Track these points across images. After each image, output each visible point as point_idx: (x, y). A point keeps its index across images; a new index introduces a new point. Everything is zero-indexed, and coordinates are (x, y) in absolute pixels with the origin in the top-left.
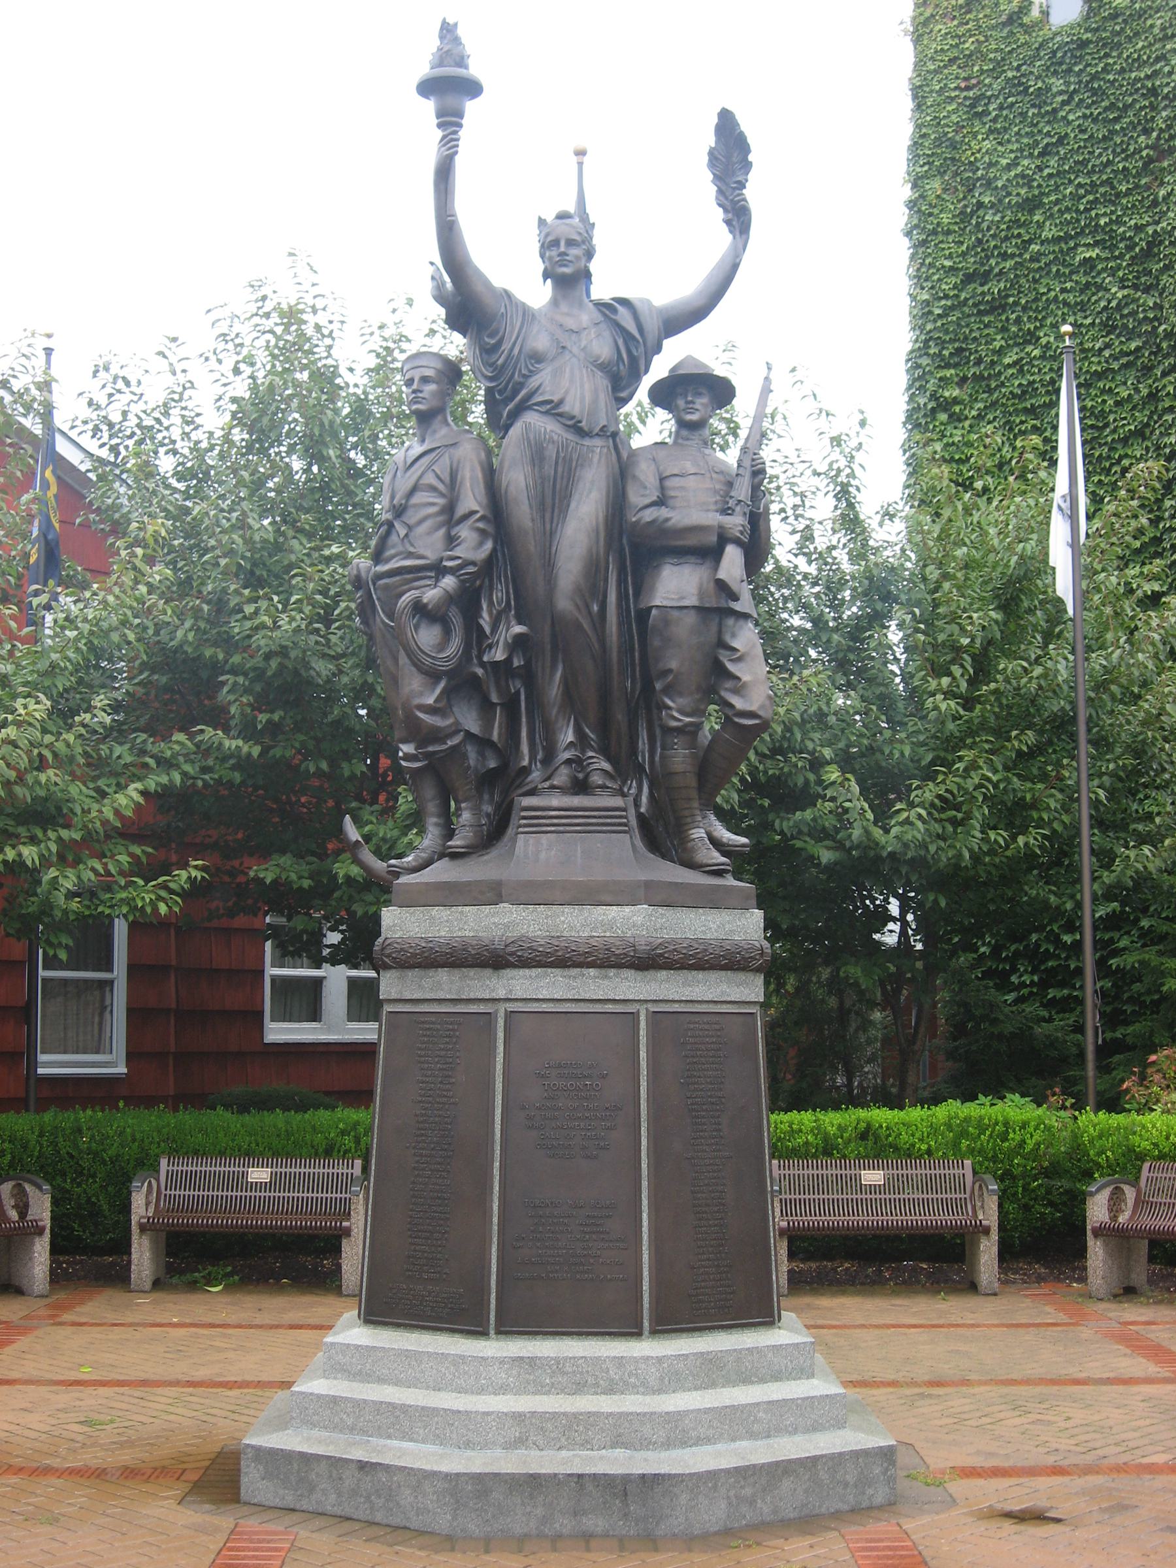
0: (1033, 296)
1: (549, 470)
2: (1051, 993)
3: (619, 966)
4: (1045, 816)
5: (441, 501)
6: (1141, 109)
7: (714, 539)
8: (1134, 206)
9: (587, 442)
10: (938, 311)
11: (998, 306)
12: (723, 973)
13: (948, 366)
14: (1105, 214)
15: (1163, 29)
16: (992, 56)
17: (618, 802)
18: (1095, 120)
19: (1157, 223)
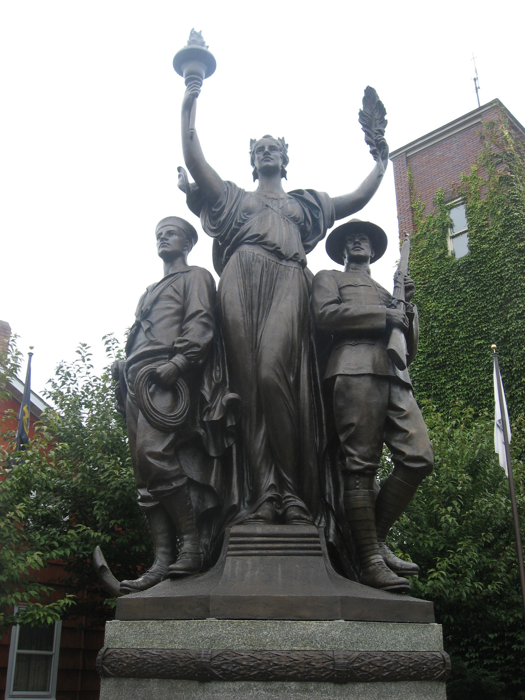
0: (456, 361)
1: (256, 280)
2: (485, 662)
3: (319, 679)
4: (499, 575)
5: (176, 306)
6: (497, 285)
7: (383, 323)
8: (497, 322)
9: (284, 263)
10: (417, 369)
11: (442, 366)
12: (412, 684)
13: (423, 391)
14: (485, 327)
15: (504, 254)
16: (434, 271)
17: (312, 530)
18: (478, 291)
19: (508, 328)
